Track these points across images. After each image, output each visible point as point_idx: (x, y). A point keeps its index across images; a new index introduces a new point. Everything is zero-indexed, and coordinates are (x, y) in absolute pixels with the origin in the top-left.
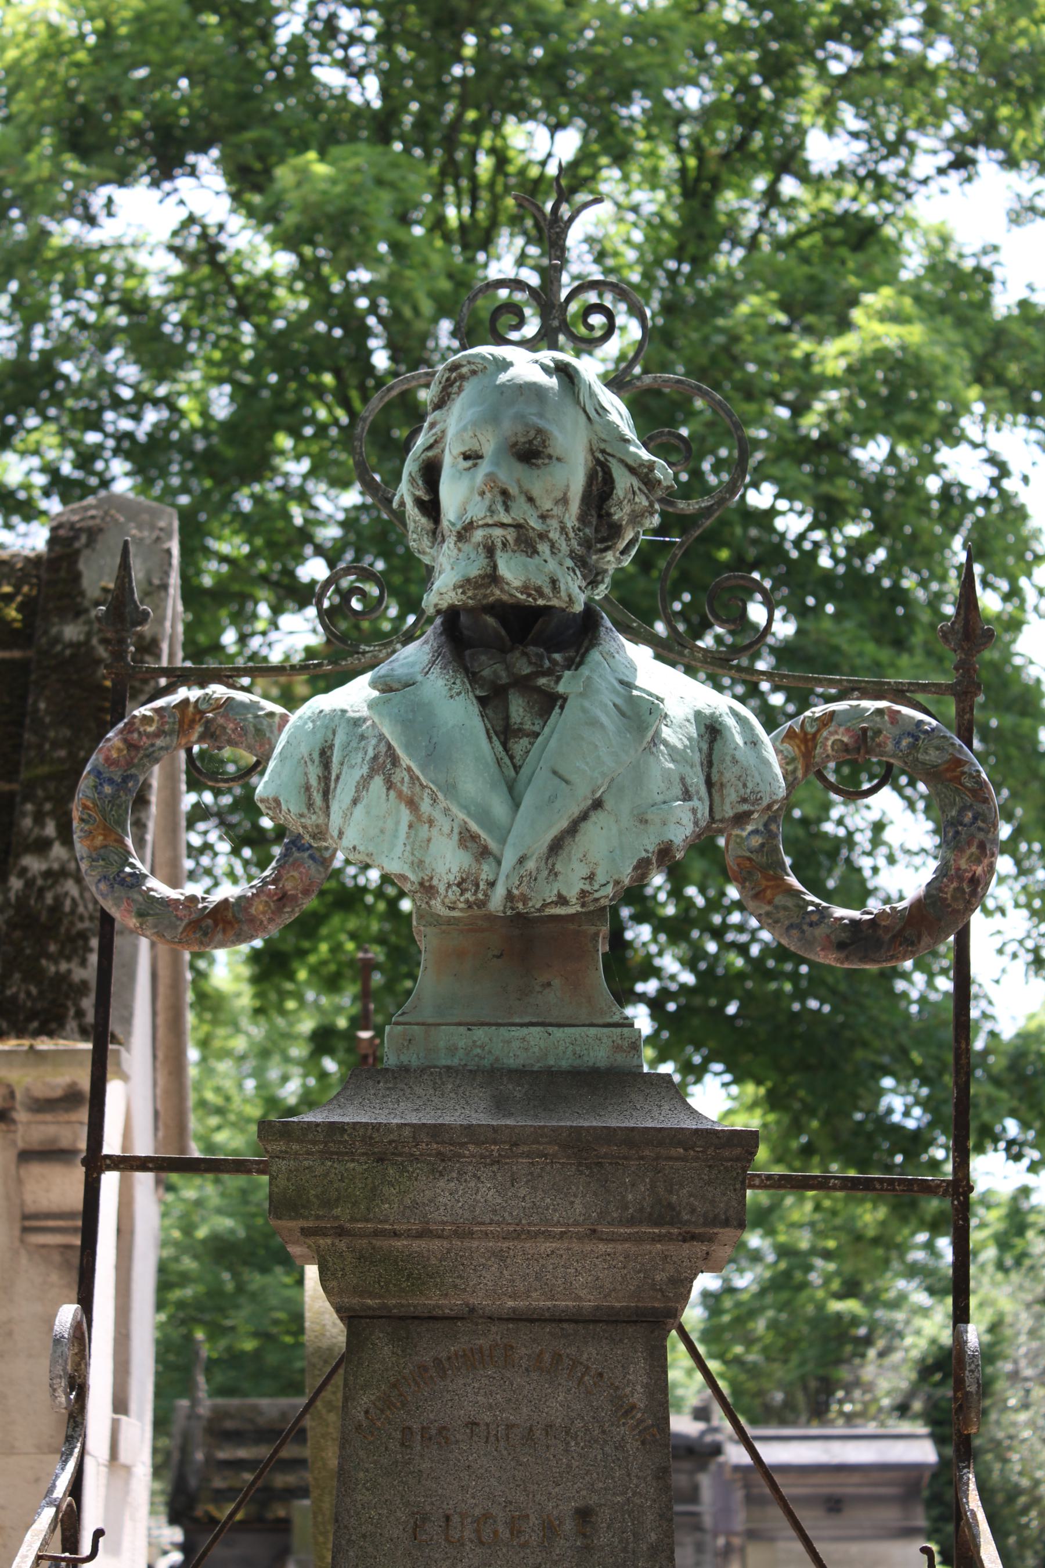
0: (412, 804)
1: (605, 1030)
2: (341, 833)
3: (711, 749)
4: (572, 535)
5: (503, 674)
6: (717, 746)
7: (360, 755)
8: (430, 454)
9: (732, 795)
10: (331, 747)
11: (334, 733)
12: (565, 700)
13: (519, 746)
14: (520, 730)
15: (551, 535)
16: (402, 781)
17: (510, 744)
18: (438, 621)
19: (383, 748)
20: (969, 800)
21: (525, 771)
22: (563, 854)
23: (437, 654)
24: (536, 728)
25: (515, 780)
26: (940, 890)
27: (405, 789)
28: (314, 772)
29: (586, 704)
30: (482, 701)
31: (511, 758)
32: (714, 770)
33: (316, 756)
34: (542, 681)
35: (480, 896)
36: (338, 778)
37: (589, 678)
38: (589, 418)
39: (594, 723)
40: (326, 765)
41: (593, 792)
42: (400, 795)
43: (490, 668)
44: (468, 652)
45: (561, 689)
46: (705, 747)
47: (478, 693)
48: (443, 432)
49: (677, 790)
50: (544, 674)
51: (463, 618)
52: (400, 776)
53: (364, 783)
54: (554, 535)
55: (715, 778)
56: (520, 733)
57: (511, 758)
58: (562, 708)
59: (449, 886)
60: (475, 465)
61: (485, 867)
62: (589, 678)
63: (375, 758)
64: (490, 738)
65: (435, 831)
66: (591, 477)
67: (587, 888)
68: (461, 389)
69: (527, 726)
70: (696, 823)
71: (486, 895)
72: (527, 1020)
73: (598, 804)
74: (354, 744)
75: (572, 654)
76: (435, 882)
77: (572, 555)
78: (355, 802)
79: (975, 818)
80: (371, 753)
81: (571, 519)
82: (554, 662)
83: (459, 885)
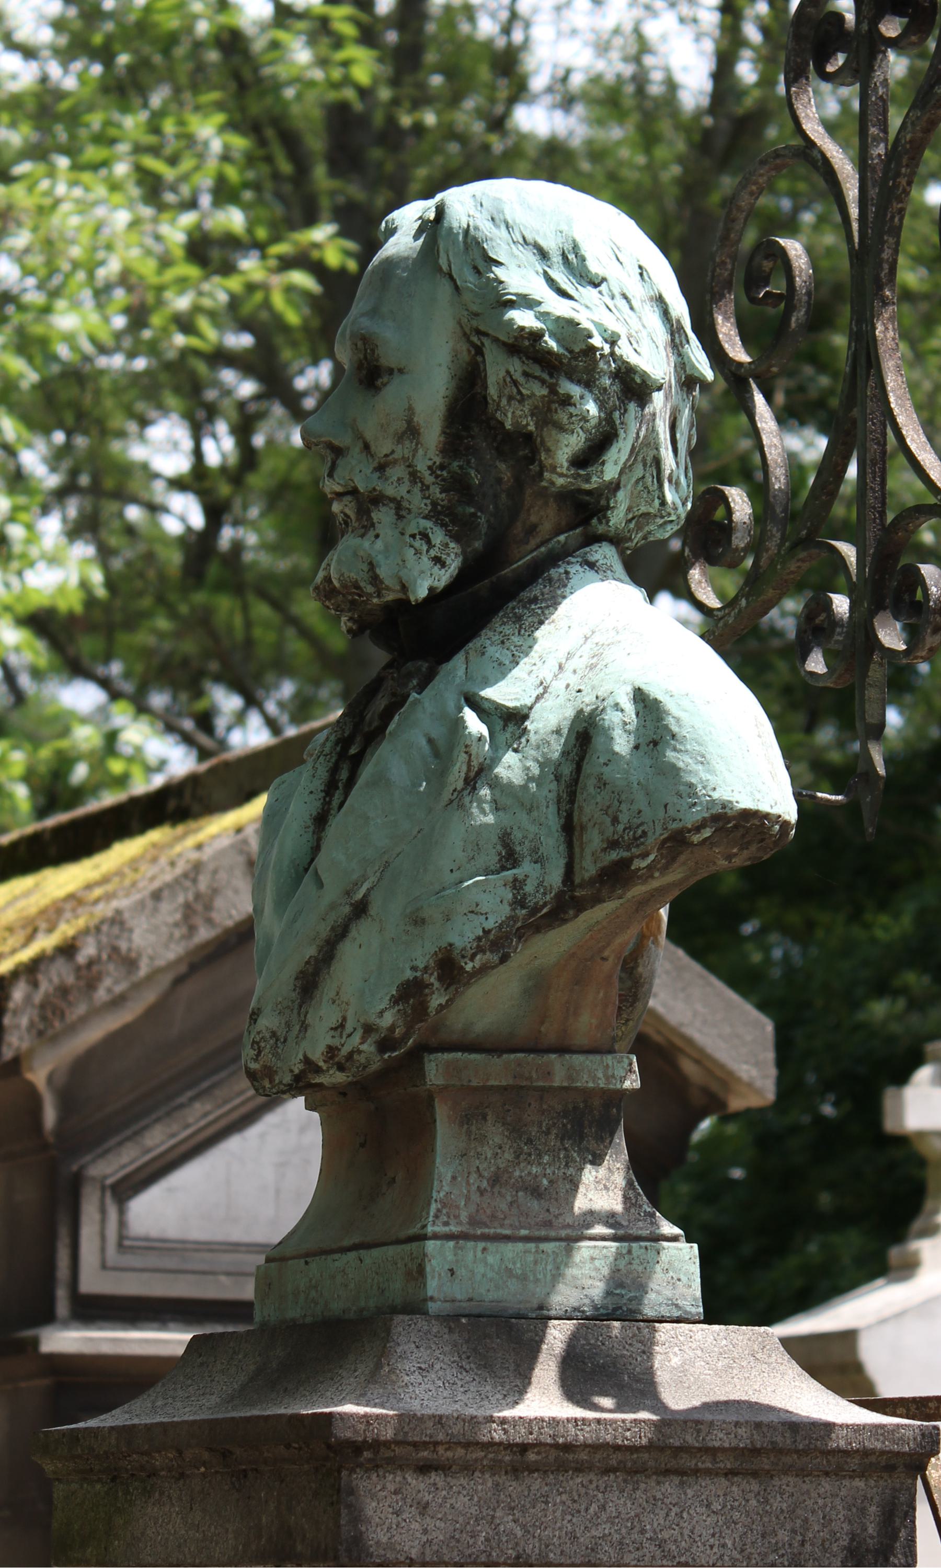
1: (399, 1248)
4: (429, 479)
9: (594, 840)
67: (336, 1042)
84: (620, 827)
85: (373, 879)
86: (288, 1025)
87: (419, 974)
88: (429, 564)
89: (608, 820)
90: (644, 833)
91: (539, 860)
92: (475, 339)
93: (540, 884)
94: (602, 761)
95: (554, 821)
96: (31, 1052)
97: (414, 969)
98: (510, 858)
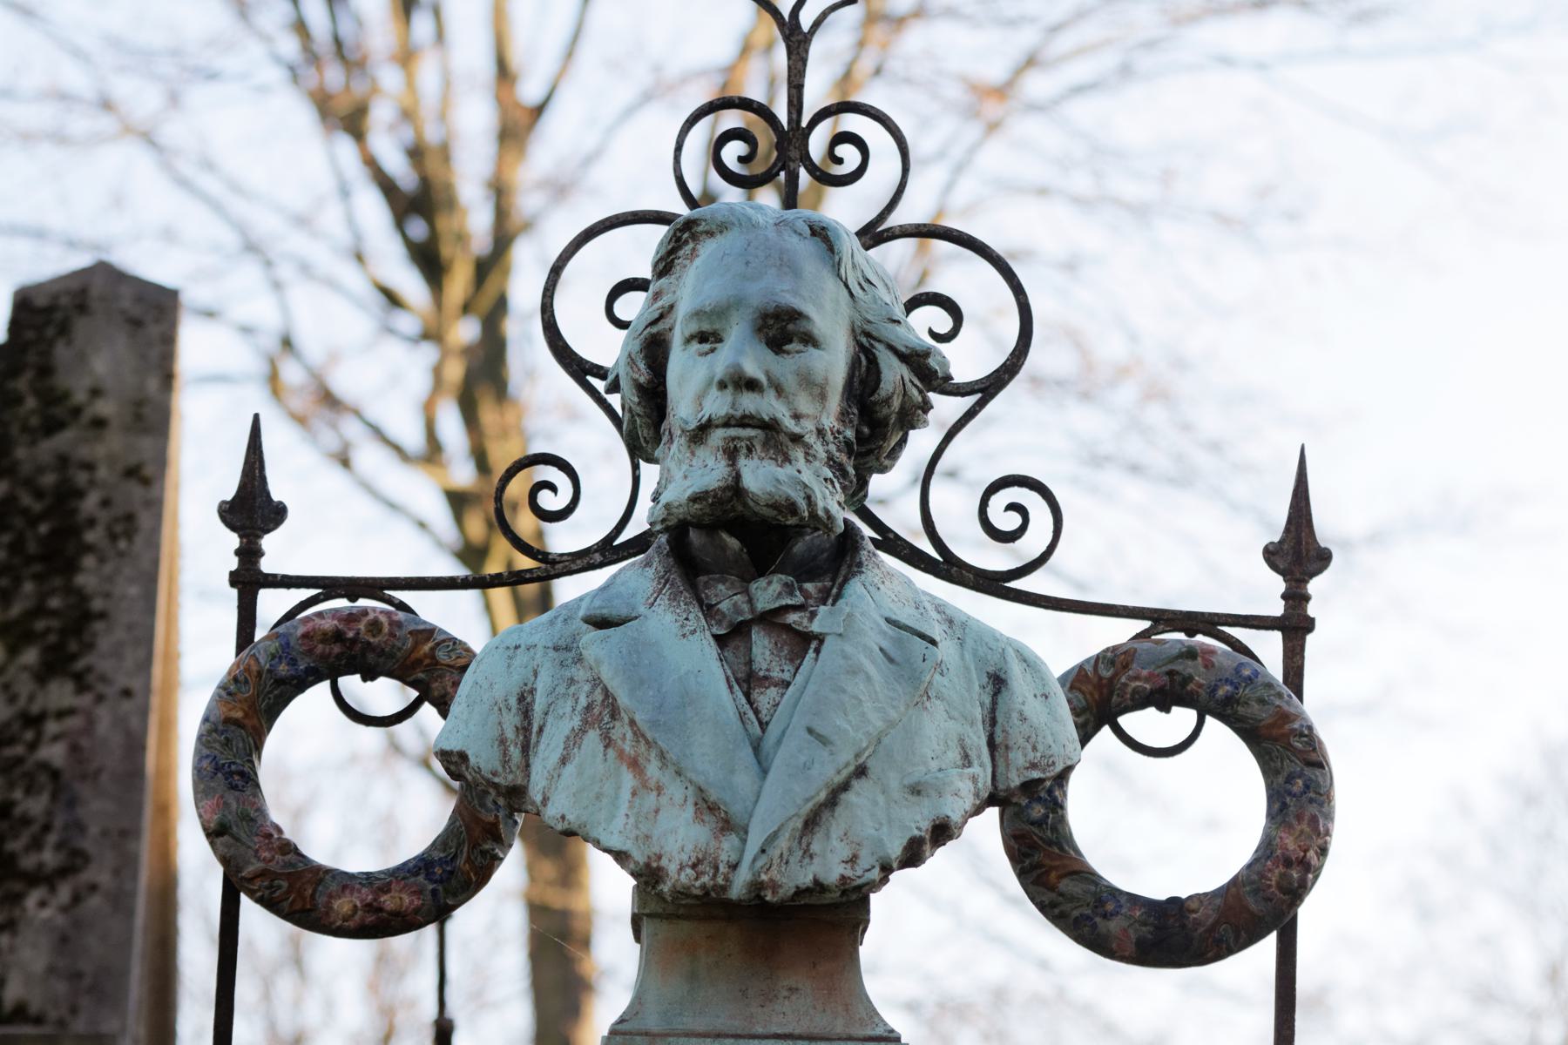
0: (635, 764)
2: (545, 800)
3: (994, 703)
5: (745, 607)
7: (570, 703)
8: (654, 330)
9: (1018, 758)
10: (532, 691)
11: (536, 674)
12: (821, 642)
13: (765, 698)
14: (766, 678)
15: (806, 439)
16: (624, 738)
17: (755, 695)
18: (663, 538)
19: (598, 696)
20: (1297, 766)
21: (774, 730)
22: (819, 836)
23: (664, 580)
24: (787, 676)
25: (760, 739)
26: (1262, 876)
28: (511, 720)
29: (849, 649)
30: (720, 640)
31: (756, 712)
32: (998, 730)
33: (513, 701)
34: (792, 618)
35: (720, 881)
36: (541, 730)
37: (850, 615)
38: (851, 295)
39: (855, 670)
40: (526, 713)
41: (857, 756)
42: (621, 754)
43: (728, 599)
44: (703, 579)
45: (816, 627)
46: (988, 700)
47: (716, 631)
48: (672, 307)
49: (954, 755)
50: (795, 608)
51: (694, 536)
52: (621, 730)
53: (577, 736)
54: (811, 439)
55: (998, 740)
56: (766, 681)
57: (756, 712)
58: (817, 651)
59: (682, 868)
60: (713, 350)
61: (726, 845)
62: (850, 615)
63: (589, 708)
64: (731, 687)
65: (664, 800)
66: (854, 365)
67: (849, 873)
68: (694, 254)
69: (776, 674)
70: (977, 795)
71: (727, 879)
72: (700, 1025)
73: (861, 772)
74: (561, 689)
75: (828, 584)
76: (664, 862)
77: (832, 462)
78: (564, 761)
79: (1307, 787)
80: (583, 702)
82: (806, 595)
83: (694, 866)
86: (790, 849)
89: (1029, 748)
92: (864, 340)
95: (983, 741)
97: (919, 829)
98: (967, 760)
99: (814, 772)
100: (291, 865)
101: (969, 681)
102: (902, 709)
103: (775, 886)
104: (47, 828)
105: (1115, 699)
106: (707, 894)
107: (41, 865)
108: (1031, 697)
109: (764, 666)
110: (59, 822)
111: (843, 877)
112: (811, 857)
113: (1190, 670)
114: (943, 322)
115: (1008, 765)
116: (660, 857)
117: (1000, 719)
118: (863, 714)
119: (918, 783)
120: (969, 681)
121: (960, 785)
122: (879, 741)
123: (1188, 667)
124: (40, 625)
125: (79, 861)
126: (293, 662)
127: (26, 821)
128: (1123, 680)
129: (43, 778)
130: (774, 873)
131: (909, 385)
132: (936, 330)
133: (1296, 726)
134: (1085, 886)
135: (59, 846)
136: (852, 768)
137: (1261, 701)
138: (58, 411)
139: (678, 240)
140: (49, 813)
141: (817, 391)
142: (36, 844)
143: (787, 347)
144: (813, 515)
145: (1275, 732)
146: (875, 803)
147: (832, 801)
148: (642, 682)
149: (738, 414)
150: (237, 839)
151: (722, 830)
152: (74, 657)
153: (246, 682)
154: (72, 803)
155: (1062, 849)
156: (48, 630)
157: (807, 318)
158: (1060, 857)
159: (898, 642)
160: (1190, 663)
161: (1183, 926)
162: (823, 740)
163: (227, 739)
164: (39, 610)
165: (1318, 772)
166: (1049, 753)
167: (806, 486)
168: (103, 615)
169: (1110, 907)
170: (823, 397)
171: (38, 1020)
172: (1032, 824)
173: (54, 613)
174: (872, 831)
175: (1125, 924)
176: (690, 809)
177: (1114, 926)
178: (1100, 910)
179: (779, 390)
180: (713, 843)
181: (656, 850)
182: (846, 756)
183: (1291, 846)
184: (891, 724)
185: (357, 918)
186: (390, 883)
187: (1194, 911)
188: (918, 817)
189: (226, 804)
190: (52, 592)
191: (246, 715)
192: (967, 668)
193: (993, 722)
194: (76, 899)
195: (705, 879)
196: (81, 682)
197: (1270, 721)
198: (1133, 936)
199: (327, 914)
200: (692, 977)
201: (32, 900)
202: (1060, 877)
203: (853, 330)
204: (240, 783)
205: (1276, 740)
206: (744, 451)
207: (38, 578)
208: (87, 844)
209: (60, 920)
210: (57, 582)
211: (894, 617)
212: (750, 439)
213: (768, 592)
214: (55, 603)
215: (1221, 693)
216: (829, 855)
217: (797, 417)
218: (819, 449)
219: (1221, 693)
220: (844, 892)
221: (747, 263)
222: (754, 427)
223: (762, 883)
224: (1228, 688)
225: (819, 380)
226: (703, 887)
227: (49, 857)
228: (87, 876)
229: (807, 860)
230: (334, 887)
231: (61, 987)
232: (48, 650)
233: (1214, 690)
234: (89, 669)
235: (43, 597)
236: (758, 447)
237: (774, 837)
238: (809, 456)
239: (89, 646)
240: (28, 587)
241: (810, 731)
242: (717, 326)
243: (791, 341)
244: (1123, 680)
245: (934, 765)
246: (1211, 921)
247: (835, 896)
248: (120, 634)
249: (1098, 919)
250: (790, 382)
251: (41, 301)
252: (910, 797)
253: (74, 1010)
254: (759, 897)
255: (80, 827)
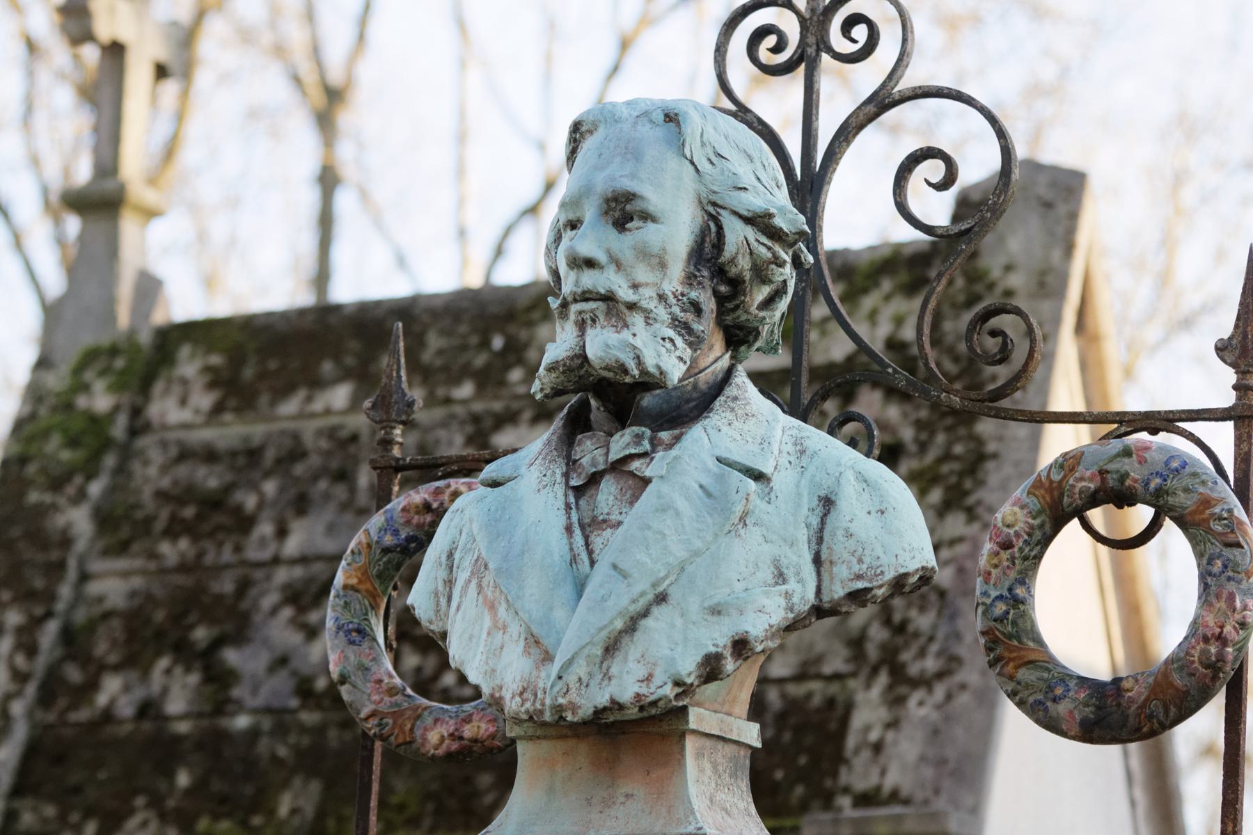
0: (492, 607)
6: (830, 520)
9: (842, 572)
14: (604, 521)
17: (592, 538)
20: (1218, 548)
22: (619, 656)
27: (489, 594)
35: (538, 706)
38: (697, 170)
46: (815, 521)
49: (767, 574)
55: (824, 556)
65: (507, 637)
67: (644, 691)
77: (677, 323)
79: (1225, 566)
81: (673, 281)
83: (521, 694)
84: (864, 567)
85: (672, 578)
86: (590, 675)
87: (719, 650)
88: (676, 361)
89: (855, 561)
90: (882, 572)
91: (801, 581)
92: (711, 209)
93: (803, 598)
94: (848, 518)
95: (808, 557)
96: (294, 673)
97: (716, 645)
98: (781, 577)
99: (610, 603)
100: (397, 705)
101: (798, 506)
102: (709, 538)
103: (574, 707)
104: (931, 639)
105: (1066, 500)
106: (531, 718)
107: (923, 671)
108: (862, 514)
109: (606, 511)
110: (940, 635)
111: (638, 695)
112: (610, 679)
113: (1127, 468)
114: (933, 170)
115: (832, 579)
116: (501, 688)
117: (826, 538)
118: (665, 548)
119: (719, 604)
120: (798, 506)
121: (766, 602)
122: (683, 569)
123: (1127, 465)
124: (945, 468)
125: (954, 665)
126: (396, 533)
127: (916, 635)
128: (1071, 482)
129: (933, 597)
130: (573, 696)
131: (754, 244)
132: (934, 181)
133: (1217, 510)
134: (1038, 674)
135: (939, 654)
136: (650, 597)
137: (1187, 490)
138: (979, 288)
139: (575, 140)
140: (935, 627)
141: (655, 261)
142: (922, 653)
143: (628, 226)
144: (644, 372)
145: (1197, 517)
146: (673, 626)
147: (633, 625)
148: (498, 535)
149: (579, 291)
150: (354, 686)
151: (544, 660)
152: (966, 493)
153: (360, 553)
154: (953, 617)
155: (1020, 642)
156: (952, 472)
157: (642, 198)
158: (1019, 649)
159: (720, 478)
160: (1126, 460)
161: (1119, 705)
162: (625, 575)
163: (346, 603)
164: (947, 457)
165: (1236, 551)
166: (875, 563)
167: (635, 348)
168: (995, 456)
169: (1059, 691)
170: (663, 265)
171: (907, 802)
172: (995, 620)
173: (957, 458)
174: (668, 652)
175: (1071, 706)
176: (522, 643)
177: (1062, 708)
178: (1051, 695)
179: (618, 265)
180: (534, 673)
181: (498, 682)
182: (642, 586)
183: (1211, 624)
184: (696, 553)
185: (444, 746)
186: (471, 715)
187: (1128, 690)
188: (717, 635)
189: (346, 658)
190: (958, 439)
191: (360, 581)
192: (799, 495)
193: (820, 540)
194: (949, 697)
195: (528, 705)
196: (971, 514)
197: (1193, 508)
198: (1078, 717)
199: (423, 745)
200: (551, 790)
201: (912, 702)
202: (1017, 667)
203: (700, 202)
204: (357, 639)
205: (1199, 525)
206: (589, 322)
207: (949, 429)
208: (962, 651)
209: (935, 716)
210: (962, 431)
211: (725, 455)
212: (592, 311)
213: (621, 444)
214: (958, 449)
215: (1152, 486)
216: (625, 676)
217: (635, 287)
218: (662, 313)
219: (1152, 486)
220: (642, 708)
221: (600, 155)
222: (595, 300)
223: (560, 705)
224: (1158, 481)
225: (656, 250)
226: (527, 712)
227: (930, 664)
228: (959, 677)
229: (606, 682)
230: (429, 721)
231: (928, 772)
232: (949, 489)
233: (1147, 484)
234: (979, 503)
235: (950, 444)
236: (602, 317)
237: (570, 663)
238: (649, 319)
239: (980, 483)
240: (941, 438)
241: (615, 567)
242: (578, 214)
243: (632, 219)
244: (1071, 482)
245: (738, 587)
246: (1143, 698)
247: (633, 713)
248: (1008, 470)
249: (1049, 704)
250: (627, 256)
251: (976, 197)
252: (710, 618)
253: (937, 791)
254: (561, 718)
255: (957, 636)
